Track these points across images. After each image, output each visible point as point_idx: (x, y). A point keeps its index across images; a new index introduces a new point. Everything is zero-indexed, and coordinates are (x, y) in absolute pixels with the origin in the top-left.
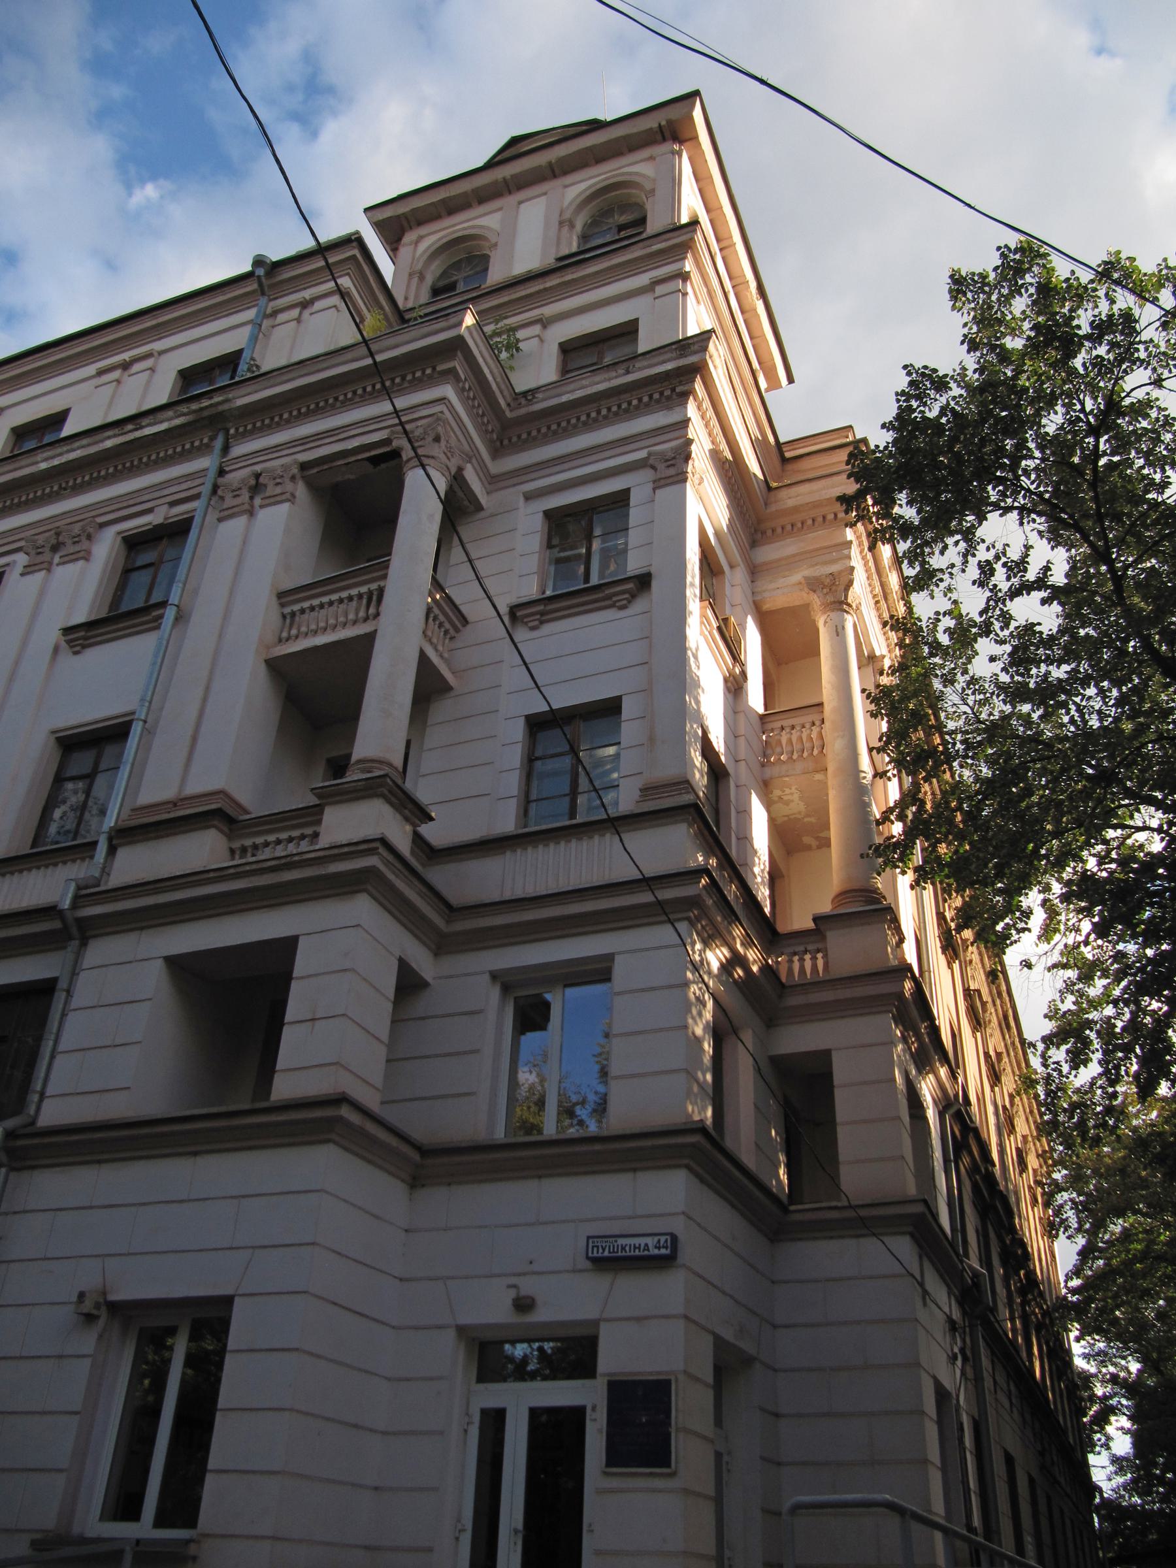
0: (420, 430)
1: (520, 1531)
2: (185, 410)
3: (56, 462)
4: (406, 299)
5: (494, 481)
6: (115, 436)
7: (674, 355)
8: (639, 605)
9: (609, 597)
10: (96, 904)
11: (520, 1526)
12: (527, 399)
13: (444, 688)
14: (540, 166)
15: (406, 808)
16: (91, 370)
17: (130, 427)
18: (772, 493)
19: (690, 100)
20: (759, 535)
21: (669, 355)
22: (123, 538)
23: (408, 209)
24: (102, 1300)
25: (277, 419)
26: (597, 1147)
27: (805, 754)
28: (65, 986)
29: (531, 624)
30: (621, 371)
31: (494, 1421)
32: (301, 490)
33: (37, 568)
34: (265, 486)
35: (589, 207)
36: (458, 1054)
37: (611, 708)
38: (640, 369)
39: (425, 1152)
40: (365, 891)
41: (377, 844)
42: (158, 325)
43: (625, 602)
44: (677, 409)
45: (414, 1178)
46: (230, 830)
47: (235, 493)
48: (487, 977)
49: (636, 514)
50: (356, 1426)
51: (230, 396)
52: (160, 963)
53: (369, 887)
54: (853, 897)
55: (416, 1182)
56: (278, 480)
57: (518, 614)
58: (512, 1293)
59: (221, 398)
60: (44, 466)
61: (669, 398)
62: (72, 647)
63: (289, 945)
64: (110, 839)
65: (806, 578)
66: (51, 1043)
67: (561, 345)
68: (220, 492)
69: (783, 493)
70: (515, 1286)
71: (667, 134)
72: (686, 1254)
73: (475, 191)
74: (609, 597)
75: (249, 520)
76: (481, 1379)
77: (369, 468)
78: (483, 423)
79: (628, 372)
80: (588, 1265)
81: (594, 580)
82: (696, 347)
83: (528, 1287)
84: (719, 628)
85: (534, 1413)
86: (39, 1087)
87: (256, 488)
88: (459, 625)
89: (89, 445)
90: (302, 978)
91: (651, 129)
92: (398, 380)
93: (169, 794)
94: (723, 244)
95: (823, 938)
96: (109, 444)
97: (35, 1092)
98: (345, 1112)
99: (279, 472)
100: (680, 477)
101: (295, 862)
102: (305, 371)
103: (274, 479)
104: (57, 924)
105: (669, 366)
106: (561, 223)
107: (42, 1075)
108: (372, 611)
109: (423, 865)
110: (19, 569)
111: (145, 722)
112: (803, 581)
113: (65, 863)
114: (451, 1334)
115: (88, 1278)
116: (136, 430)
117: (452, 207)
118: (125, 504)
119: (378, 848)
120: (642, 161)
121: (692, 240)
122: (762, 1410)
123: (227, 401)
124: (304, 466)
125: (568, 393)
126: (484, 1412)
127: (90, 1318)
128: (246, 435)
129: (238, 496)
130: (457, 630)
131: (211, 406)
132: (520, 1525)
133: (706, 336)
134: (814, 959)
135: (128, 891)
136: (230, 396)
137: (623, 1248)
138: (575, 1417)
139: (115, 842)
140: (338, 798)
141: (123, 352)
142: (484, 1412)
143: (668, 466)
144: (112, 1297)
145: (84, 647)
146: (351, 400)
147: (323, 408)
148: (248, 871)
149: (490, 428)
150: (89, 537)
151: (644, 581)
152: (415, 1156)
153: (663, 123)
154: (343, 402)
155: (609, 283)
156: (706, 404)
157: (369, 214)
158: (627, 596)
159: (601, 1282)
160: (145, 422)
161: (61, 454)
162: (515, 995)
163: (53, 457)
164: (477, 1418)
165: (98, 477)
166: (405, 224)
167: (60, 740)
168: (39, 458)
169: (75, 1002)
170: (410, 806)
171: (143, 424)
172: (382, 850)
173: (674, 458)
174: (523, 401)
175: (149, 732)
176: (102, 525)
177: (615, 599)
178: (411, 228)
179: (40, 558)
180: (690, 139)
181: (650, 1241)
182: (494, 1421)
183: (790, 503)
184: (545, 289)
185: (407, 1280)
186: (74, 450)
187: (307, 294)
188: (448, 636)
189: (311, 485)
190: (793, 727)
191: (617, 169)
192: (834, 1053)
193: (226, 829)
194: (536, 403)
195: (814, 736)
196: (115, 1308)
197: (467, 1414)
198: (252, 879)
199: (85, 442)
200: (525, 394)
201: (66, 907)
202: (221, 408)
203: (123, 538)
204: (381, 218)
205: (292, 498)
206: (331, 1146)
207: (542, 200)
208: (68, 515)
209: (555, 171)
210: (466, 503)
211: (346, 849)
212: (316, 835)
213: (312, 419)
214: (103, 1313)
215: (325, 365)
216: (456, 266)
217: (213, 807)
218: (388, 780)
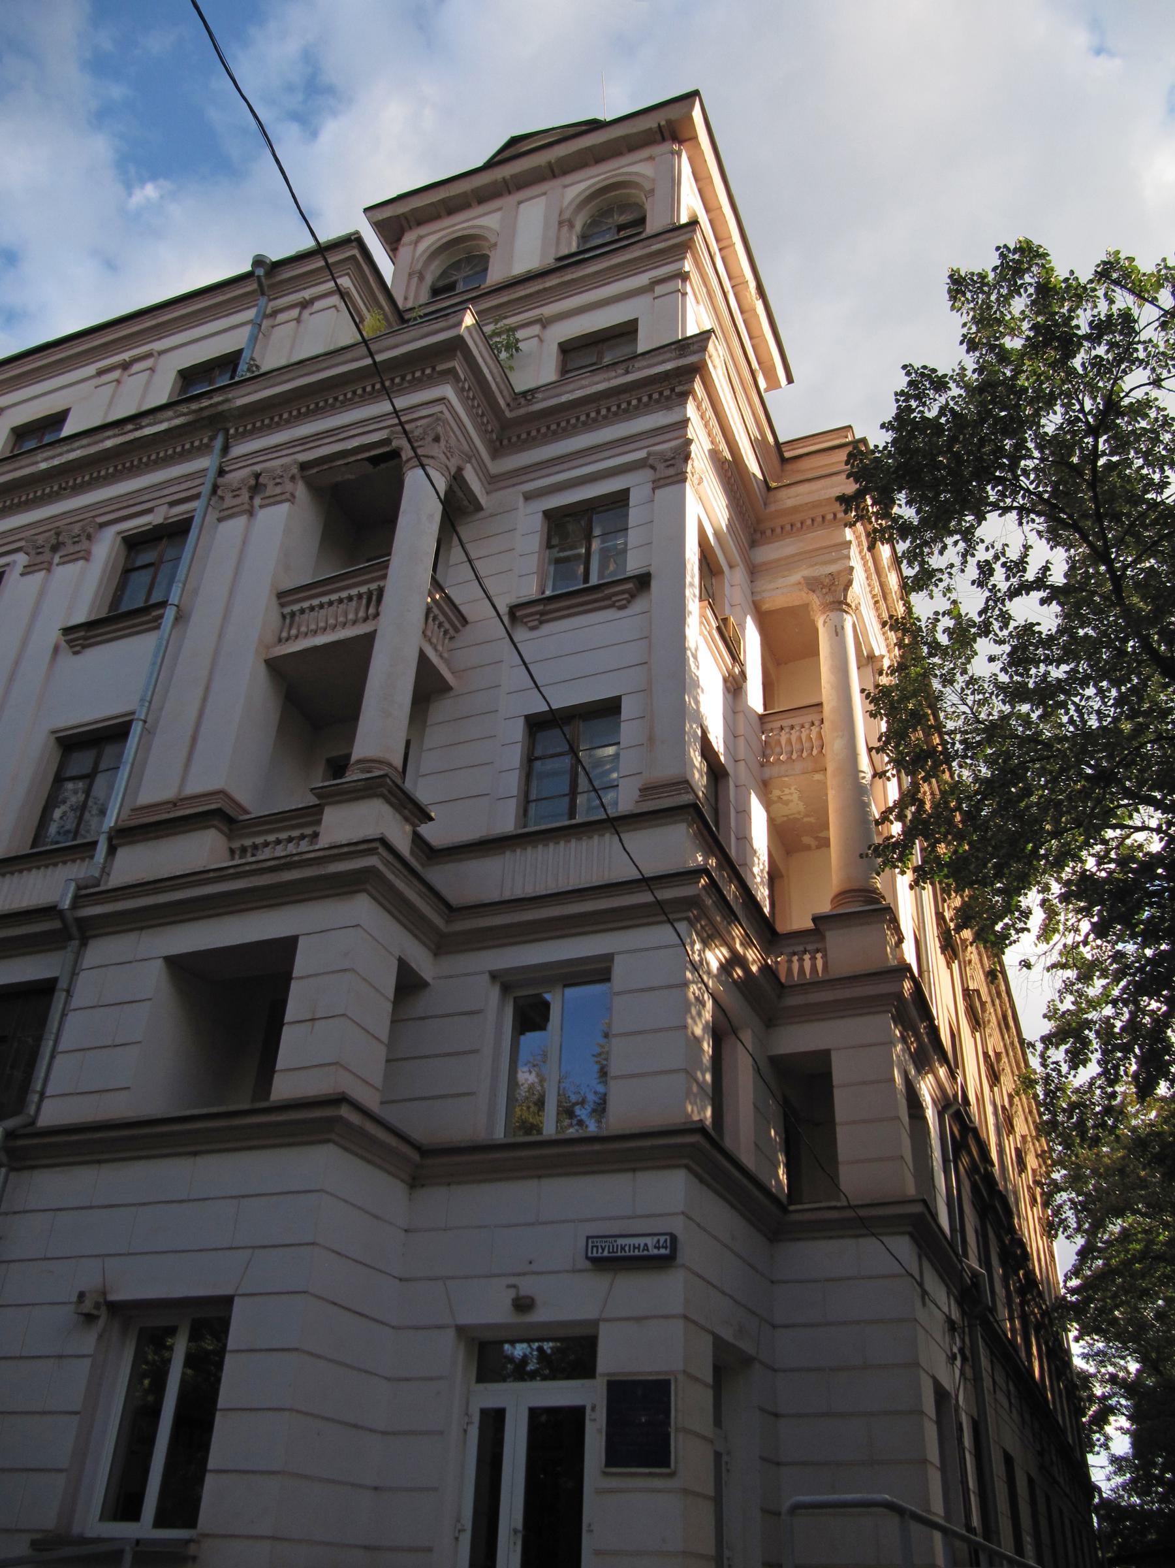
0: (420, 430)
2: (185, 410)
3: (56, 462)
4: (406, 299)
5: (493, 481)
6: (115, 436)
7: (673, 355)
8: (639, 605)
9: (609, 597)
11: (520, 1526)
12: (526, 399)
13: (444, 688)
14: (540, 166)
15: (405, 808)
16: (91, 370)
17: (130, 427)
18: (772, 493)
19: (690, 100)
21: (669, 355)
22: (123, 538)
24: (102, 1300)
25: (276, 419)
26: (597, 1147)
30: (620, 371)
31: (494, 1421)
32: (301, 490)
33: (36, 568)
34: (265, 486)
36: (458, 1054)
37: (610, 708)
38: (640, 369)
39: (425, 1152)
40: (365, 891)
42: (158, 325)
43: (624, 602)
44: (677, 409)
45: (414, 1179)
46: (230, 830)
47: (235, 493)
48: (486, 977)
49: (635, 514)
50: (355, 1426)
51: (230, 396)
52: (160, 963)
53: (369, 887)
55: (415, 1182)
56: (278, 480)
57: (517, 614)
58: (512, 1293)
59: (221, 398)
60: (43, 466)
61: (668, 398)
63: (287, 947)
64: (110, 839)
65: (805, 578)
66: (51, 1043)
67: (561, 345)
68: (220, 492)
69: (783, 493)
70: (514, 1286)
71: (666, 134)
72: (686, 1254)
73: (475, 191)
74: (609, 597)
76: (480, 1380)
77: (369, 468)
78: (483, 423)
79: (627, 372)
80: (588, 1264)
81: (594, 580)
82: (695, 347)
83: (528, 1286)
84: (719, 628)
85: (534, 1413)
86: (39, 1087)
87: (256, 488)
88: (459, 625)
89: (89, 445)
90: (302, 978)
91: (650, 129)
92: (397, 380)
93: (169, 794)
95: (823, 938)
98: (345, 1112)
99: (279, 472)
100: (679, 477)
101: (295, 862)
102: (305, 371)
103: (274, 479)
104: (56, 924)
105: (669, 366)
106: (561, 223)
107: (42, 1075)
108: (372, 611)
109: (423, 865)
110: (19, 569)
111: (145, 722)
112: (802, 581)
113: (65, 863)
114: (451, 1334)
116: (136, 430)
118: (125, 504)
119: (377, 848)
120: (641, 161)
121: (692, 240)
123: (227, 401)
124: (304, 466)
125: (568, 393)
126: (484, 1412)
127: (90, 1318)
128: (245, 435)
129: (238, 495)
130: (457, 630)
131: (211, 406)
133: (705, 336)
134: (813, 959)
135: (128, 891)
136: (230, 396)
137: (623, 1248)
138: (575, 1417)
139: (115, 842)
140: (337, 798)
142: (484, 1412)
144: (112, 1297)
145: (84, 647)
146: (351, 400)
147: (323, 408)
148: (248, 871)
149: (489, 428)
150: (89, 537)
151: (643, 581)
152: (416, 1156)
153: (663, 123)
156: (706, 404)
157: (369, 214)
159: (599, 1283)
160: (144, 422)
161: (61, 454)
162: (515, 995)
163: (53, 457)
164: (476, 1418)
167: (59, 740)
168: (39, 458)
169: (75, 1002)
170: (410, 806)
171: (143, 424)
172: (381, 850)
173: (673, 458)
174: (523, 401)
175: (149, 732)
176: (102, 525)
177: (614, 599)
178: (410, 228)
179: (40, 558)
181: (650, 1241)
182: (494, 1421)
183: (790, 503)
184: (545, 289)
185: (407, 1280)
186: (73, 450)
187: (307, 294)
188: (448, 636)
189: (310, 485)
190: (792, 727)
191: (616, 169)
192: (832, 1052)
193: (226, 829)
194: (536, 403)
196: (115, 1308)
197: (467, 1414)
198: (252, 879)
199: (85, 442)
200: (524, 394)
201: (66, 907)
202: (220, 408)
203: (123, 538)
204: (380, 218)
205: (292, 498)
206: (331, 1146)
208: (68, 515)
209: (555, 171)
210: (466, 503)
212: (316, 835)
214: (103, 1313)
215: (324, 365)
216: (456, 266)
217: (213, 807)
218: (388, 780)
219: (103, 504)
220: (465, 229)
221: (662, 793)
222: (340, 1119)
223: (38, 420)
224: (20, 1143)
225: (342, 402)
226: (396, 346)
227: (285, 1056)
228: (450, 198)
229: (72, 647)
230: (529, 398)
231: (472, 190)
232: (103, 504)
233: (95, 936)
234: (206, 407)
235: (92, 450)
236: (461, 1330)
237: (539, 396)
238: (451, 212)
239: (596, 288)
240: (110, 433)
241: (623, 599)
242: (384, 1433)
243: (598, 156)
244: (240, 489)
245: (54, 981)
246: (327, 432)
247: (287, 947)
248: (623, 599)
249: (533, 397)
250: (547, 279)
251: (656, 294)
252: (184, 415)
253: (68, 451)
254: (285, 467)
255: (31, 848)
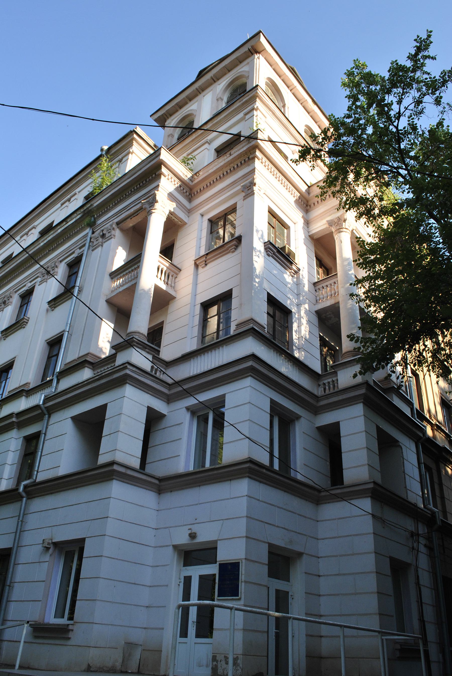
0: (152, 199)
1: (195, 622)
3: (45, 242)
9: (228, 249)
10: (49, 402)
11: (195, 621)
12: (197, 176)
15: (146, 348)
16: (59, 205)
17: (64, 223)
18: (310, 188)
19: (259, 35)
20: (309, 207)
21: (244, 144)
22: (67, 264)
23: (165, 111)
24: (50, 542)
25: (108, 208)
26: (215, 472)
27: (329, 297)
28: (44, 432)
29: (202, 266)
31: (188, 580)
33: (43, 282)
34: (105, 234)
35: (229, 89)
36: (174, 441)
39: (161, 480)
40: (127, 383)
41: (250, 363)
42: (77, 182)
43: (233, 250)
44: (252, 165)
45: (159, 491)
46: (93, 367)
48: (185, 409)
53: (128, 381)
54: (347, 355)
56: (109, 231)
58: (189, 532)
59: (89, 205)
60: (42, 244)
62: (51, 308)
63: (223, 396)
64: (57, 377)
65: (327, 221)
66: (40, 453)
68: (92, 240)
71: (253, 51)
73: (187, 97)
75: (102, 248)
76: (184, 566)
79: (230, 155)
83: (195, 528)
85: (201, 577)
86: (36, 469)
87: (103, 236)
88: (178, 272)
89: (54, 233)
90: (108, 419)
91: (246, 51)
94: (291, 88)
96: (59, 231)
97: (35, 471)
98: (116, 467)
100: (252, 193)
101: (103, 376)
103: (108, 231)
104: (40, 411)
106: (217, 100)
107: (37, 464)
109: (165, 369)
110: (38, 283)
111: (68, 332)
113: (47, 388)
114: (171, 548)
115: (46, 535)
116: (66, 224)
117: (180, 106)
118: (67, 252)
119: (127, 366)
120: (245, 65)
121: (257, 93)
122: (306, 573)
123: (92, 205)
125: (211, 169)
126: (185, 577)
128: (100, 216)
129: (98, 240)
130: (177, 274)
132: (195, 620)
133: (256, 132)
135: (57, 395)
140: (120, 349)
141: (67, 196)
142: (185, 577)
143: (248, 190)
144: (53, 541)
145: (55, 308)
146: (131, 194)
147: (122, 199)
148: (90, 382)
149: (185, 191)
150: (57, 267)
152: (157, 482)
153: (250, 48)
154: (128, 195)
155: (230, 120)
156: (265, 159)
157: (152, 117)
158: (234, 247)
160: (68, 220)
161: (46, 239)
162: (198, 415)
163: (44, 240)
164: (182, 580)
165: (59, 244)
166: (166, 117)
167: (48, 343)
169: (48, 437)
170: (148, 347)
172: (129, 367)
173: (250, 186)
175: (70, 335)
176: (61, 261)
178: (168, 118)
179: (44, 278)
180: (263, 50)
182: (188, 580)
185: (158, 529)
186: (50, 236)
187: (120, 157)
188: (174, 277)
190: (327, 286)
191: (237, 71)
193: (91, 367)
194: (200, 176)
195: (335, 288)
196: (56, 544)
198: (92, 384)
201: (41, 404)
202: (90, 209)
203: (67, 264)
206: (114, 481)
207: (211, 93)
208: (52, 260)
209: (215, 80)
210: (180, 223)
211: (121, 367)
212: (115, 365)
213: (120, 204)
214: (52, 546)
215: (120, 183)
217: (84, 360)
218: (134, 339)
219: (60, 254)
220: (186, 112)
221: (241, 326)
222: (114, 471)
223: (46, 227)
224: (29, 489)
225: (128, 195)
226: (141, 169)
227: (102, 451)
228: (179, 102)
229: (51, 308)
230: (197, 175)
231: (186, 97)
232: (60, 254)
233: (53, 413)
234: (86, 209)
235: (55, 235)
236: (175, 547)
237: (201, 173)
238: (181, 107)
239: (226, 123)
240: (59, 227)
241: (232, 249)
242: (150, 586)
243: (229, 69)
244: (98, 237)
245: (40, 431)
246: (124, 208)
247: (223, 396)
248: (232, 249)
249: (199, 174)
250: (208, 125)
251: (246, 119)
252: (80, 214)
253: (48, 237)
254: (111, 225)
255: (41, 382)
